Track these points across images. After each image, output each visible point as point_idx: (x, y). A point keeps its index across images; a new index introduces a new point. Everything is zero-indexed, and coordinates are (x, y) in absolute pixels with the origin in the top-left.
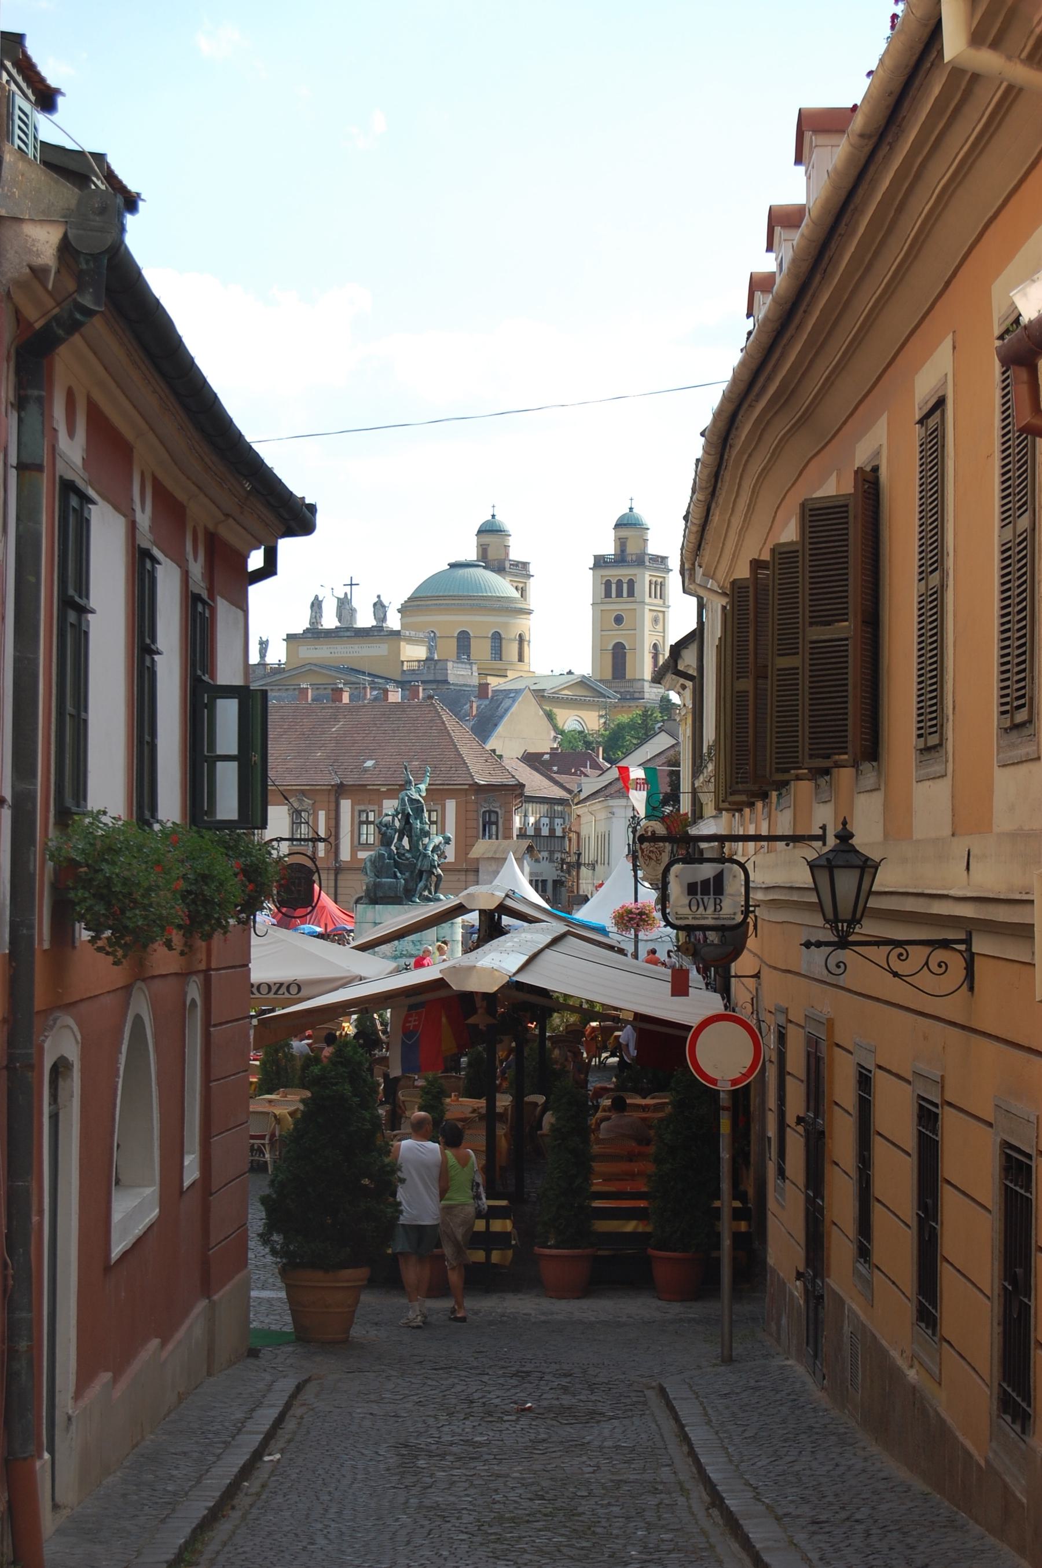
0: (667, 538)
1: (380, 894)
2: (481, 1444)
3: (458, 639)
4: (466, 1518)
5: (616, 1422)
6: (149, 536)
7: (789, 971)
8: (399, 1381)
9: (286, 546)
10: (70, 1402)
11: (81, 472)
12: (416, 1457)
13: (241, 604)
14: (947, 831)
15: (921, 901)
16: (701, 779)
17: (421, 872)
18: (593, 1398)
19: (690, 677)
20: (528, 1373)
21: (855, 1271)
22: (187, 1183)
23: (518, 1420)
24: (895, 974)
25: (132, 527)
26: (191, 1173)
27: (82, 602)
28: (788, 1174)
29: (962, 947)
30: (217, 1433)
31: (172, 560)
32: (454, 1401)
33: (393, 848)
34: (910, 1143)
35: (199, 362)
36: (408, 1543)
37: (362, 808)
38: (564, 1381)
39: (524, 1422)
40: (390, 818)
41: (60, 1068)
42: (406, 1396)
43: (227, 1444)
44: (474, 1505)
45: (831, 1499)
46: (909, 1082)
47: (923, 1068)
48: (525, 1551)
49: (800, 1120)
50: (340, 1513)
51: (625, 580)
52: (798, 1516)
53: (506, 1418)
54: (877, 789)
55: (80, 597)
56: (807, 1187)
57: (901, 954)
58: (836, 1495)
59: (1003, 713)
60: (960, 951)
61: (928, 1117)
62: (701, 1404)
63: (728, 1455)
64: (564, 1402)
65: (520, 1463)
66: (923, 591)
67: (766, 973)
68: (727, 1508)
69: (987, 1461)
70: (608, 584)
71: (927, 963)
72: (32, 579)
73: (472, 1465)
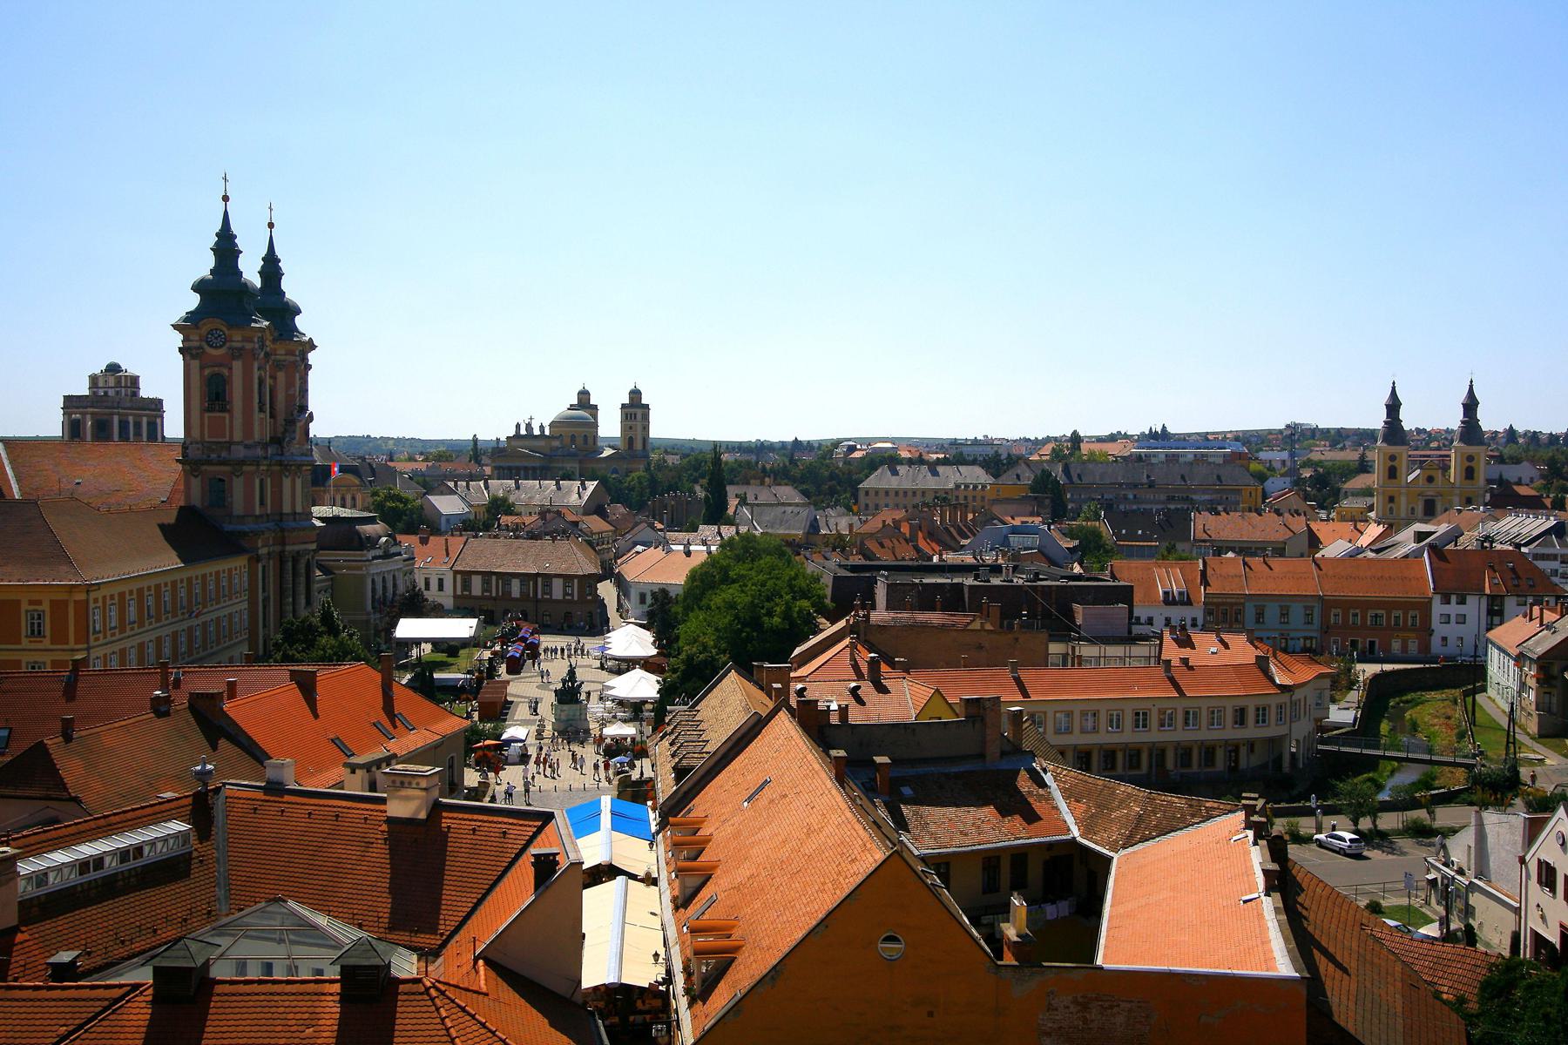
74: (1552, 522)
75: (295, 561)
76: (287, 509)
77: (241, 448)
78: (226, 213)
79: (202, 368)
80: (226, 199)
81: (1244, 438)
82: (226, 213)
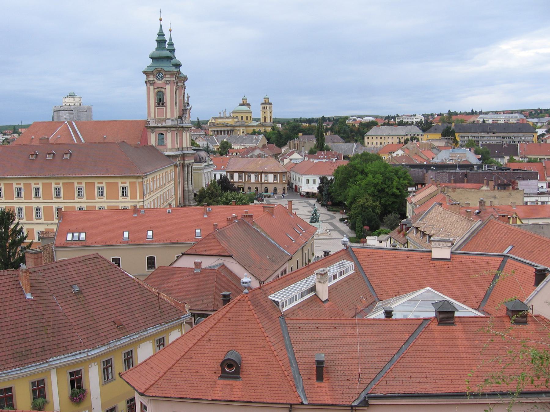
74: (286, 161)
75: (188, 166)
76: (184, 146)
77: (170, 121)
78: (161, 26)
79: (155, 89)
80: (161, 20)
81: (295, 120)
82: (161, 26)
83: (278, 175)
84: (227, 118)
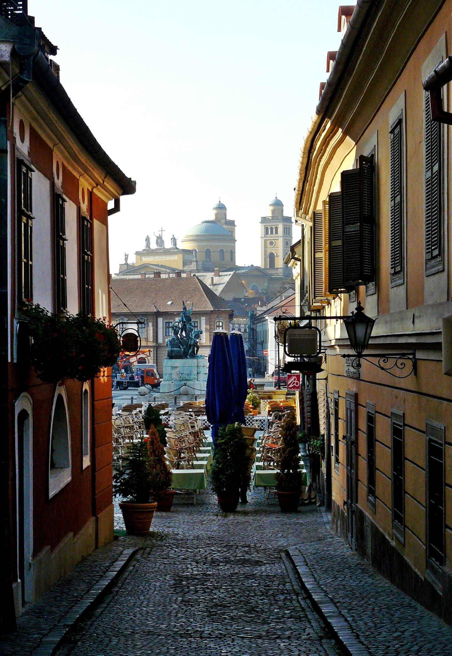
0: (289, 210)
1: (173, 355)
2: (209, 575)
3: (206, 252)
4: (202, 605)
5: (268, 565)
6: (61, 189)
7: (339, 375)
8: (177, 550)
9: (124, 199)
10: (31, 558)
11: (27, 158)
12: (182, 581)
13: (105, 222)
14: (404, 308)
15: (393, 338)
16: (304, 301)
17: (190, 346)
18: (258, 555)
19: (299, 260)
20: (232, 546)
21: (368, 500)
22: (84, 467)
23: (226, 565)
24: (382, 369)
25: (53, 185)
26: (86, 462)
27: (29, 213)
28: (340, 461)
29: (411, 357)
30: (98, 572)
31: (73, 201)
32: (199, 558)
33: (179, 336)
34: (389, 443)
35: (79, 111)
36: (176, 616)
37: (167, 321)
38: (246, 549)
39: (228, 566)
40: (177, 324)
41: (24, 414)
42: (179, 556)
43: (101, 576)
44: (205, 600)
45: (358, 595)
46: (389, 417)
47: (395, 410)
48: (225, 618)
49: (344, 437)
50: (148, 605)
51: (274, 227)
52: (344, 603)
53: (221, 564)
54: (375, 293)
55: (28, 211)
56: (347, 465)
57: (385, 360)
58: (360, 594)
59: (427, 253)
60: (411, 359)
61: (398, 433)
62: (304, 557)
63: (315, 578)
64: (246, 558)
65: (226, 583)
66: (393, 205)
67: (330, 376)
68: (313, 599)
69: (425, 578)
70: (267, 229)
71: (396, 364)
72: (4, 200)
73: (205, 583)
83: (203, 319)
84: (167, 252)
